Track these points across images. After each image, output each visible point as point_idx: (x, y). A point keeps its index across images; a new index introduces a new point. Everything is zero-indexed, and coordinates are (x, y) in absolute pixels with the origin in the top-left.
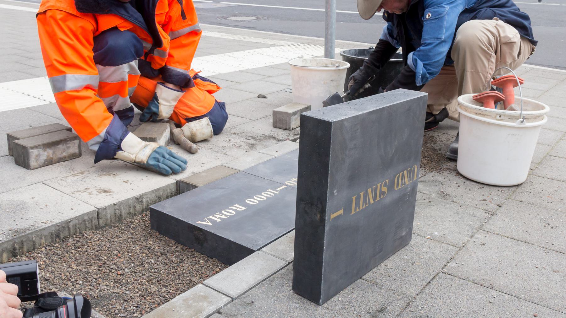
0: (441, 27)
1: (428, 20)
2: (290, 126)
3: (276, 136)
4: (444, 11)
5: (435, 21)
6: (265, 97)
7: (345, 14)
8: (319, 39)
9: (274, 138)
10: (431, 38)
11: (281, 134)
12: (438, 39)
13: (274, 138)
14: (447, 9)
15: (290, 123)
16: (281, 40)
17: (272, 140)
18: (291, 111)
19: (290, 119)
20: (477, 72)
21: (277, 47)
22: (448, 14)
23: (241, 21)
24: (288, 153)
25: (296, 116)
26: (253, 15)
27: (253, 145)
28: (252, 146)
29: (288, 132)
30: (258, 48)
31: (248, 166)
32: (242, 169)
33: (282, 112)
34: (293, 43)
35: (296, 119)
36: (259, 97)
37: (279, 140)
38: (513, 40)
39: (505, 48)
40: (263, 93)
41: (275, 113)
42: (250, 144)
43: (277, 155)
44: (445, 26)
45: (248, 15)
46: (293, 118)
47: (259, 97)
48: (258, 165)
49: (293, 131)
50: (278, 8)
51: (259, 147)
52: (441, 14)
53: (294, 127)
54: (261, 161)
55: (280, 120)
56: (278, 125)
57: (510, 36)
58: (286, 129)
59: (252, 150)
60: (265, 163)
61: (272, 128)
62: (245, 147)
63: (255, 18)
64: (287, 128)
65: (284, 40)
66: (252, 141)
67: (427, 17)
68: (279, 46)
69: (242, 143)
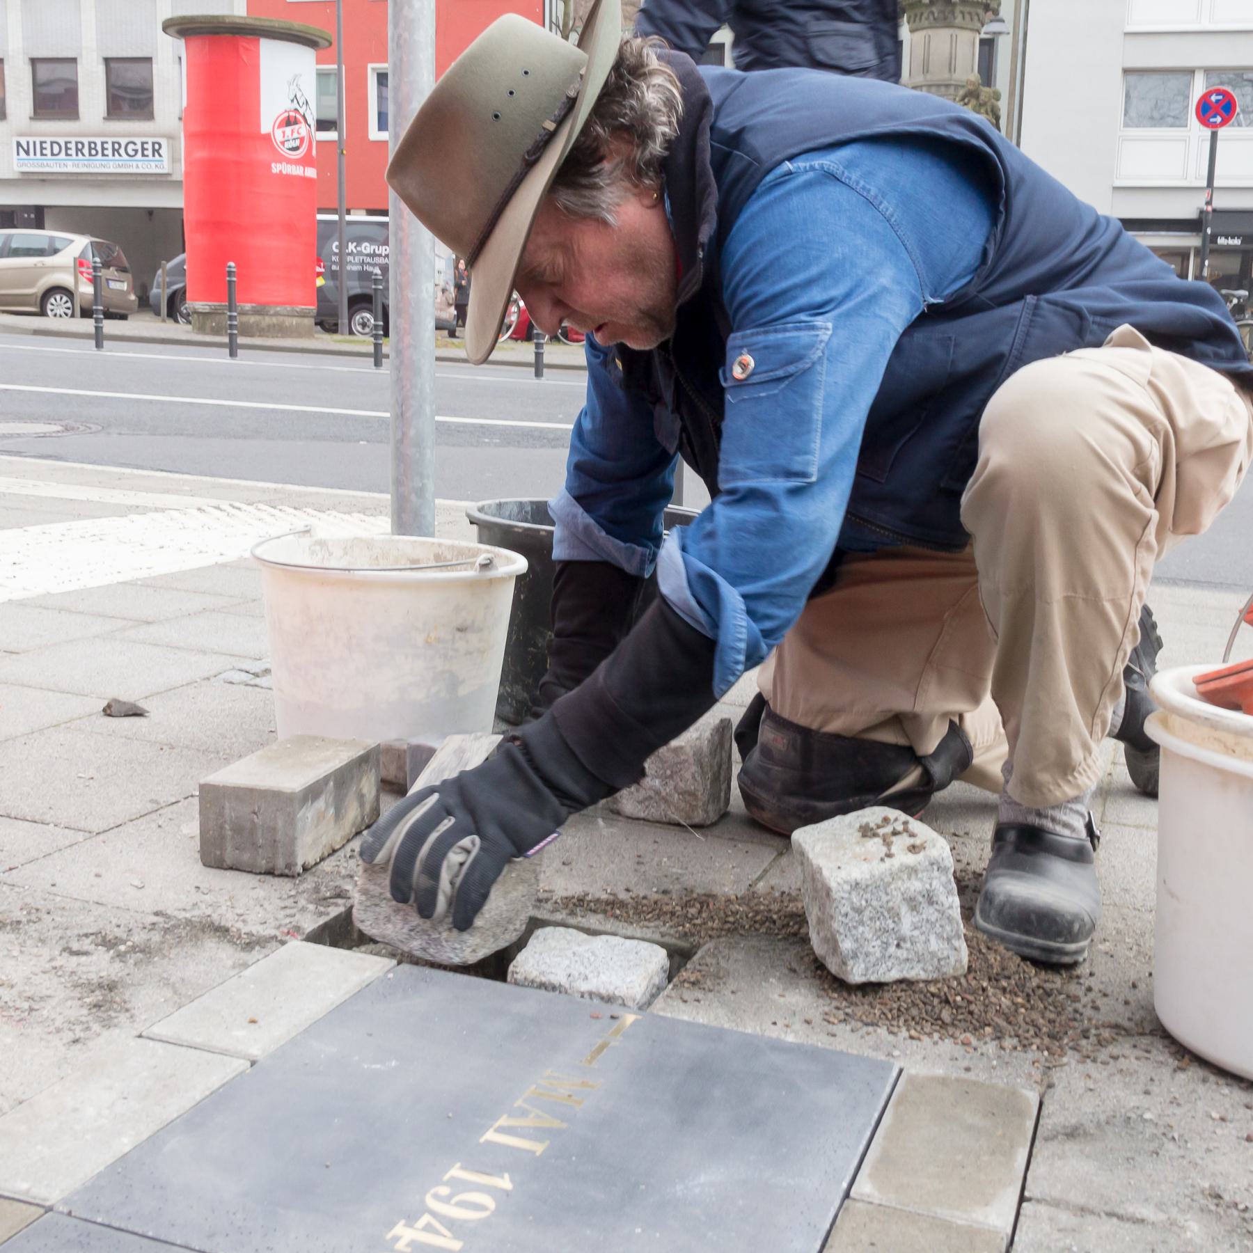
0: (801, 420)
1: (741, 384)
2: (292, 854)
3: (229, 920)
4: (810, 346)
5: (775, 390)
6: (137, 713)
7: (367, 420)
8: (302, 488)
9: (221, 931)
10: (759, 471)
11: (249, 901)
12: (789, 474)
13: (221, 931)
14: (824, 336)
15: (293, 840)
16: (167, 491)
17: (212, 947)
18: (293, 781)
19: (291, 821)
20: (1090, 589)
21: (158, 516)
22: (834, 356)
23: (11, 436)
24: (316, 1028)
25: (320, 804)
26: (49, 420)
27: (112, 987)
28: (106, 999)
29: (286, 886)
30: (79, 517)
31: (95, 1162)
32: (53, 1194)
33: (251, 791)
34: (215, 502)
35: (321, 817)
36: (108, 711)
37: (251, 943)
38: (1228, 435)
39: (1198, 471)
40: (129, 694)
41: (211, 797)
42: (91, 987)
43: (258, 1044)
44: (818, 417)
45: (34, 418)
46: (308, 814)
47: (108, 711)
48: (154, 1142)
49: (309, 882)
50: (137, 401)
51: (145, 998)
52: (797, 358)
53: (311, 858)
54: (175, 1107)
55: (238, 830)
56: (230, 856)
57: (1214, 415)
58: (270, 873)
59: (107, 1024)
60: (197, 1118)
61: (197, 872)
62: (66, 1007)
63: (59, 428)
64: (277, 870)
65: (177, 492)
66: (100, 964)
67: (737, 372)
68: (163, 510)
69: (46, 985)
